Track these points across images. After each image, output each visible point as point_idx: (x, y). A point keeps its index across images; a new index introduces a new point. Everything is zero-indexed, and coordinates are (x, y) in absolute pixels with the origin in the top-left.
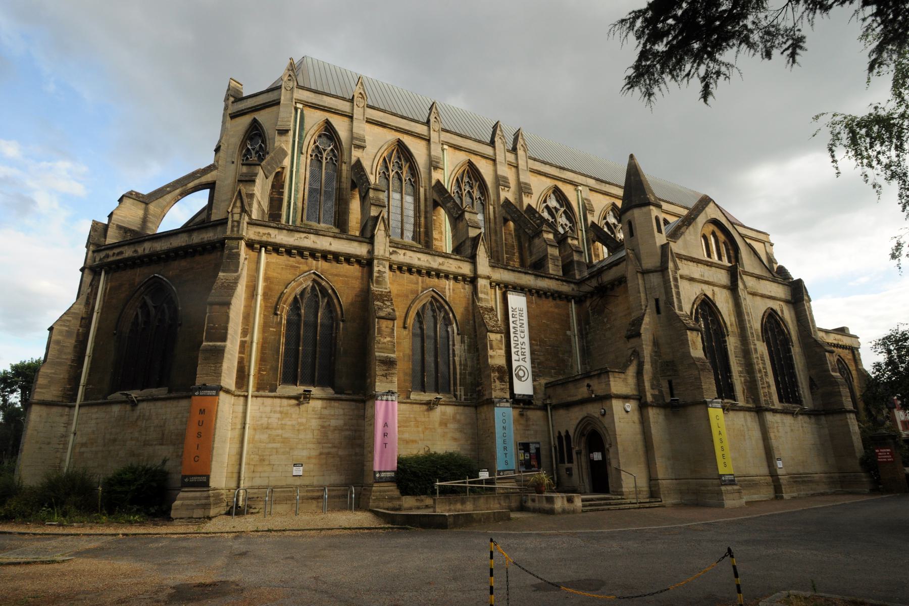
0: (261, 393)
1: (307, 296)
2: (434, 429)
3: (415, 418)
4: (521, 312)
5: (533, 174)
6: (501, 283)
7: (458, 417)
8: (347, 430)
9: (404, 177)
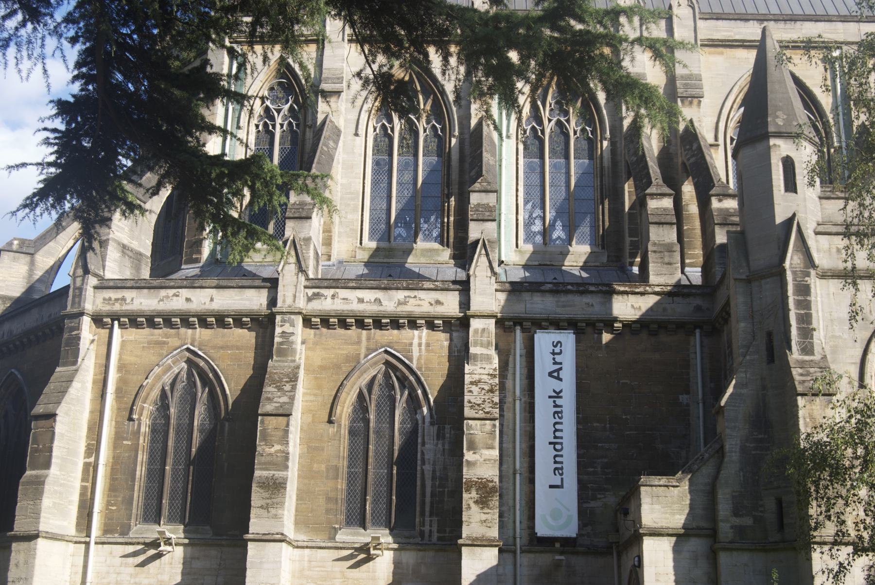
0: (110, 538)
1: (180, 386)
5: (712, 49)
6: (527, 319)
7: (423, 570)
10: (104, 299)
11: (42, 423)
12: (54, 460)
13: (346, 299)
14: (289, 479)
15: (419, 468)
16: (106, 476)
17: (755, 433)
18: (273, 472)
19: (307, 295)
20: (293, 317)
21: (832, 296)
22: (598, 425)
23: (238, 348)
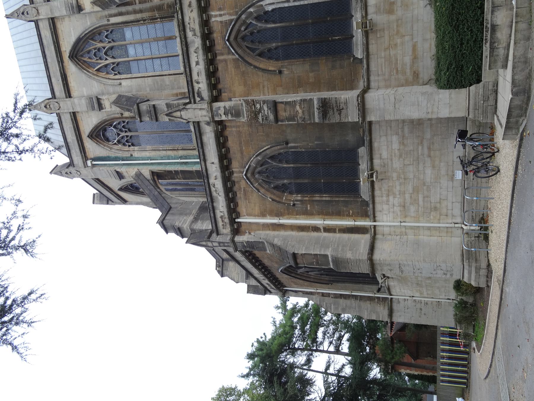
0: (370, 213)
2: (397, 20)
8: (403, 131)
10: (223, 228)
11: (299, 261)
12: (322, 253)
13: (198, 73)
14: (319, 97)
16: (331, 219)
18: (316, 110)
19: (200, 101)
20: (214, 109)
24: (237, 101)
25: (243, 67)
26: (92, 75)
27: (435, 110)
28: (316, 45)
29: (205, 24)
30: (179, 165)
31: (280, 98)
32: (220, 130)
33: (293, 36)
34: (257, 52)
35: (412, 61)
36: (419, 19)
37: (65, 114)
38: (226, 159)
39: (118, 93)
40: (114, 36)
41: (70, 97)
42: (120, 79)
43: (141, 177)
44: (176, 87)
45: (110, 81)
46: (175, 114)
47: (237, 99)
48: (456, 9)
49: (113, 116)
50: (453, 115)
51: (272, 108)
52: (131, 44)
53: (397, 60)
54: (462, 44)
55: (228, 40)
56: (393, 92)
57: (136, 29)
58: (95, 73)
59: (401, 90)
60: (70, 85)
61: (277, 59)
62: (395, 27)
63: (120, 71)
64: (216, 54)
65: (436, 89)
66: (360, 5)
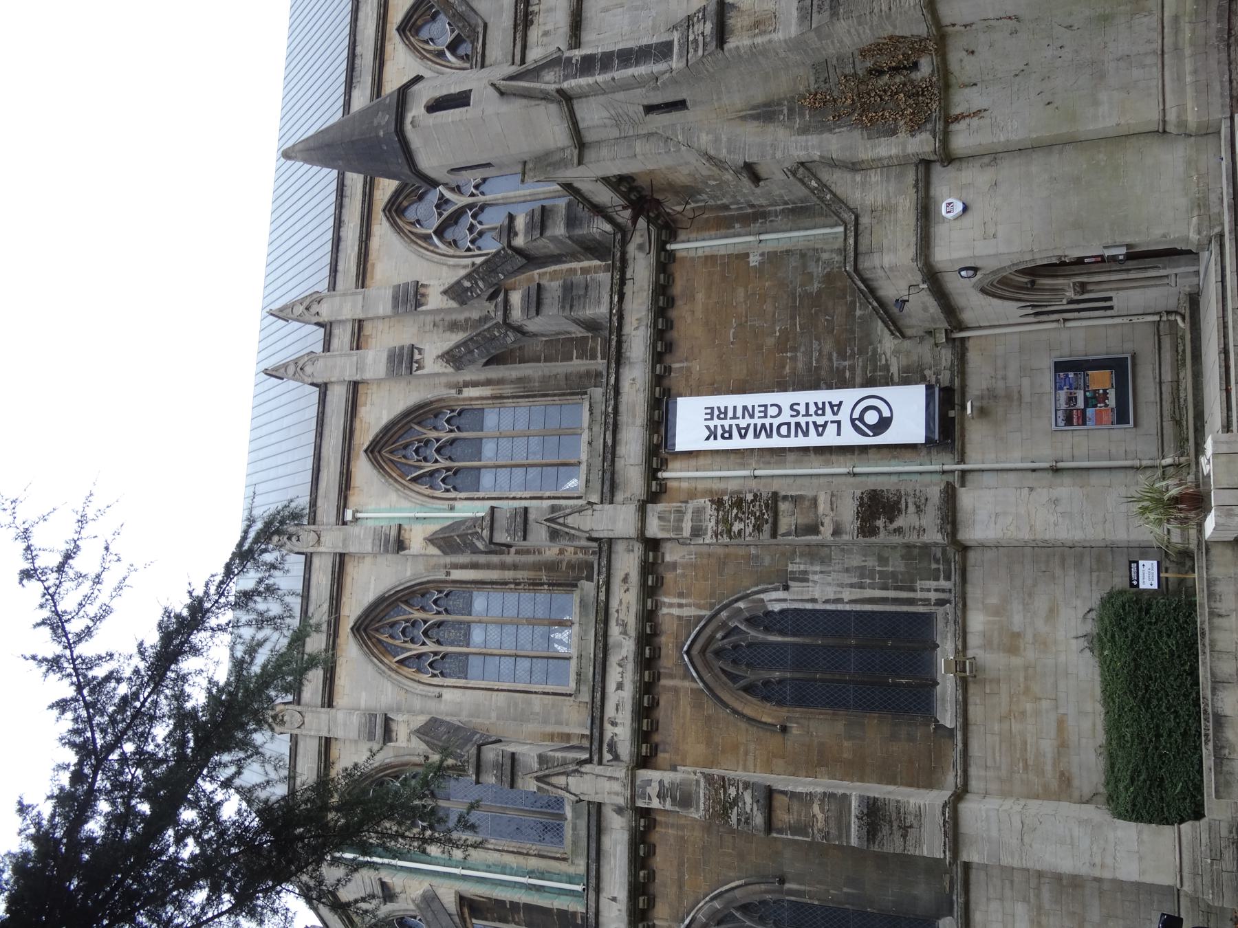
2: (1026, 668)
3: (1001, 719)
4: (716, 412)
8: (1038, 896)
9: (445, 436)
13: (617, 705)
15: (848, 607)
17: (782, 117)
18: (853, 819)
20: (638, 782)
21: (601, 36)
22: (788, 367)
23: (681, 864)
24: (689, 773)
25: (710, 708)
26: (386, 670)
27: (1109, 861)
28: (860, 689)
29: (648, 616)
30: (523, 891)
31: (780, 782)
32: (642, 829)
33: (817, 664)
34: (742, 683)
35: (1056, 750)
36: (1070, 671)
37: (308, 739)
38: (643, 894)
39: (429, 713)
40: (450, 603)
41: (330, 705)
42: (442, 686)
43: (435, 905)
44: (553, 720)
45: (421, 687)
46: (554, 780)
47: (689, 769)
48: (1142, 669)
49: (406, 759)
50: (1148, 879)
51: (762, 801)
52: (480, 622)
53: (1026, 743)
54: (1158, 736)
55: (688, 652)
56: (1018, 808)
57: (496, 596)
58: (394, 666)
59: (1034, 805)
60: (337, 682)
61: (781, 703)
62: (1022, 679)
63: (444, 671)
64: (659, 674)
65: (1108, 817)
66: (953, 629)
